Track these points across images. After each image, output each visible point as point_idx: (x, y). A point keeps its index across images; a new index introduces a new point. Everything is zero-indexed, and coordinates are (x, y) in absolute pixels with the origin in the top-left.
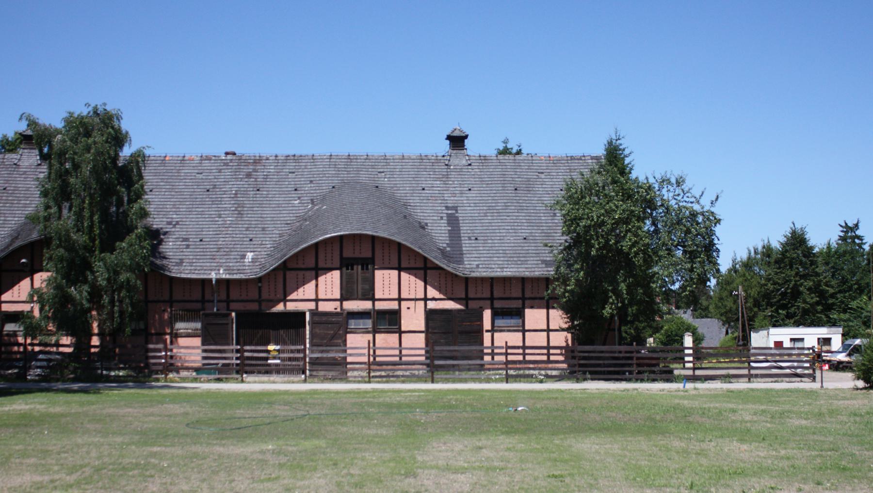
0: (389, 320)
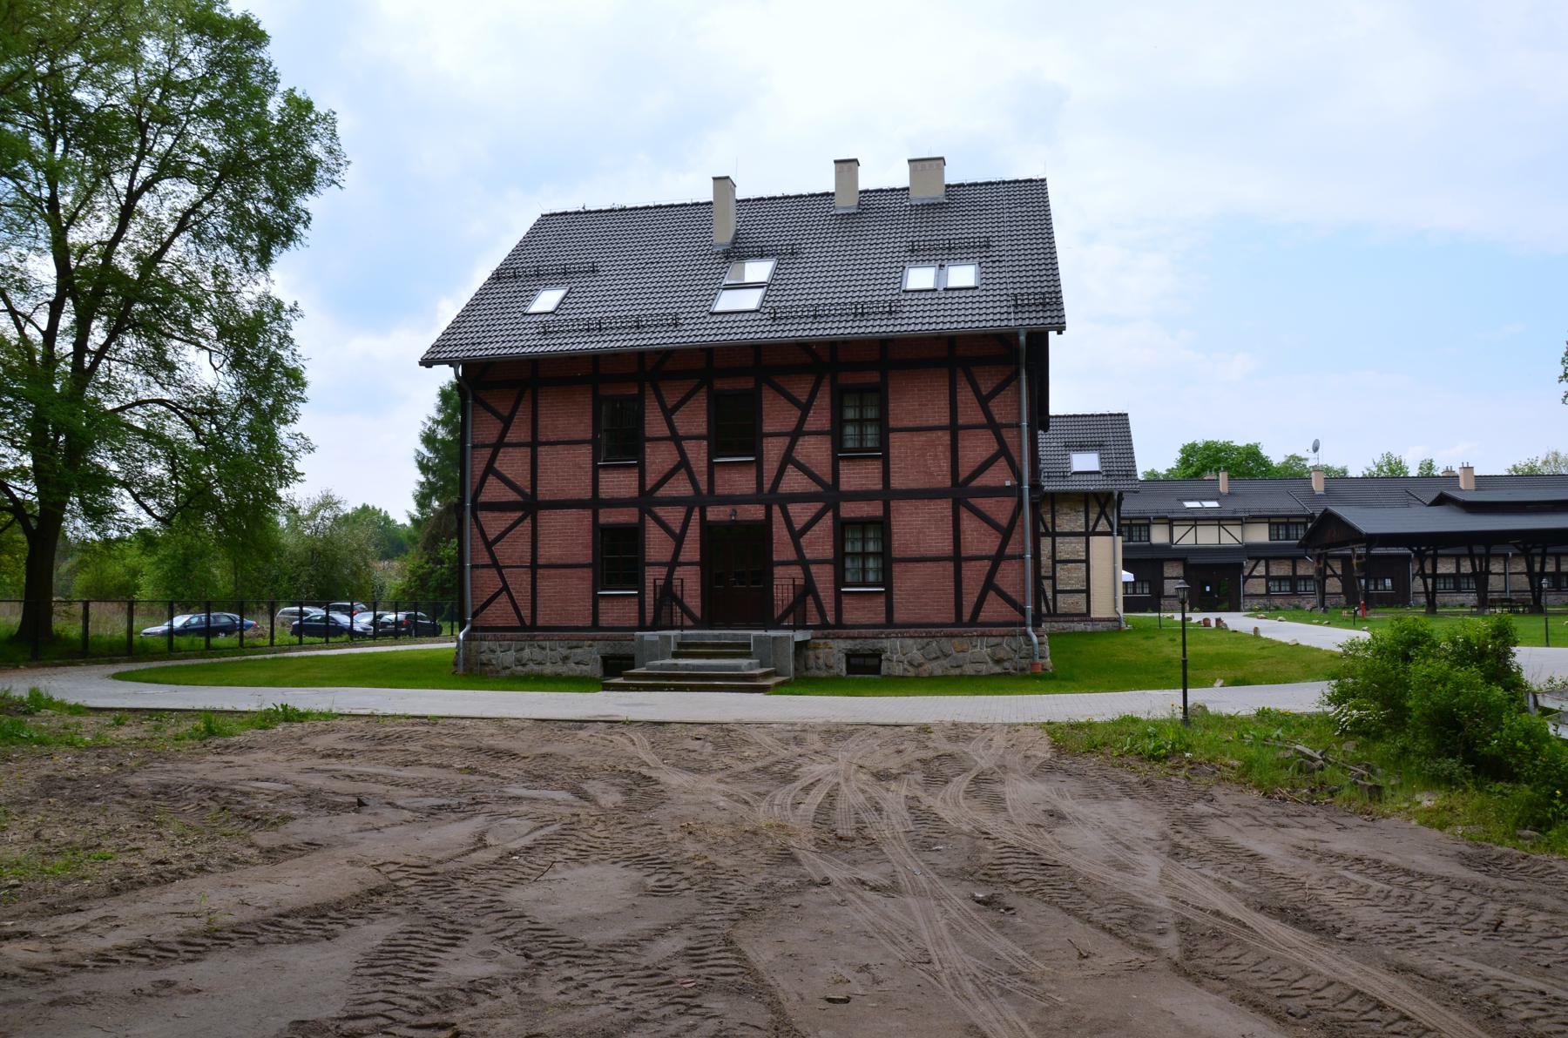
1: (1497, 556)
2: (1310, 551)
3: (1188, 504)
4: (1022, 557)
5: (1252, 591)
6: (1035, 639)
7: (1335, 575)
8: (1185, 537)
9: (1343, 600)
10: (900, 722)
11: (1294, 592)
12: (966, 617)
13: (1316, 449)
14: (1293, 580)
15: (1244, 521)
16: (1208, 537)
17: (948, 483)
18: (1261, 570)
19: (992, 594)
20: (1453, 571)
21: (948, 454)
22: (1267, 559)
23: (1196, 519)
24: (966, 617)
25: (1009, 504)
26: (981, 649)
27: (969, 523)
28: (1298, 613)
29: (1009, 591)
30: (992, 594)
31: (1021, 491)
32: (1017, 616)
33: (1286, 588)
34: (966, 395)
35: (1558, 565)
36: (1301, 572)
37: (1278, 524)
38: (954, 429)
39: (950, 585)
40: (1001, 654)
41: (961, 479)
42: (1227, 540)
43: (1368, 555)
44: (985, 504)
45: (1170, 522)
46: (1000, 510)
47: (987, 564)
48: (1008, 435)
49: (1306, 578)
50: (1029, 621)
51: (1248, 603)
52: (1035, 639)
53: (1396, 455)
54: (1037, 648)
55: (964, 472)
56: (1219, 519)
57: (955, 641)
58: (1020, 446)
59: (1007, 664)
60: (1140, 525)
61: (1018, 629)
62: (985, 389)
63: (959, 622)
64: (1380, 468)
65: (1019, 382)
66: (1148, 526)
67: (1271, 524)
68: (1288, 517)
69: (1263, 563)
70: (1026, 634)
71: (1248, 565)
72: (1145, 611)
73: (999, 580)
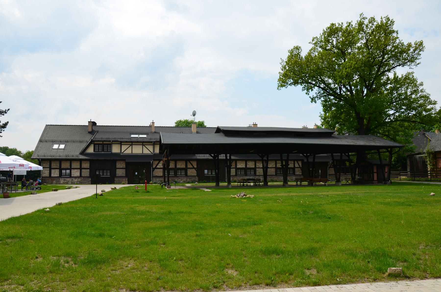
3: (132, 136)
5: (157, 175)
7: (194, 168)
8: (127, 150)
9: (197, 179)
13: (194, 115)
16: (137, 150)
20: (244, 166)
23: (132, 142)
33: (243, 172)
36: (179, 166)
42: (146, 152)
45: (121, 143)
49: (181, 169)
51: (154, 180)
60: (108, 144)
66: (111, 145)
68: (103, 141)
72: (209, 182)
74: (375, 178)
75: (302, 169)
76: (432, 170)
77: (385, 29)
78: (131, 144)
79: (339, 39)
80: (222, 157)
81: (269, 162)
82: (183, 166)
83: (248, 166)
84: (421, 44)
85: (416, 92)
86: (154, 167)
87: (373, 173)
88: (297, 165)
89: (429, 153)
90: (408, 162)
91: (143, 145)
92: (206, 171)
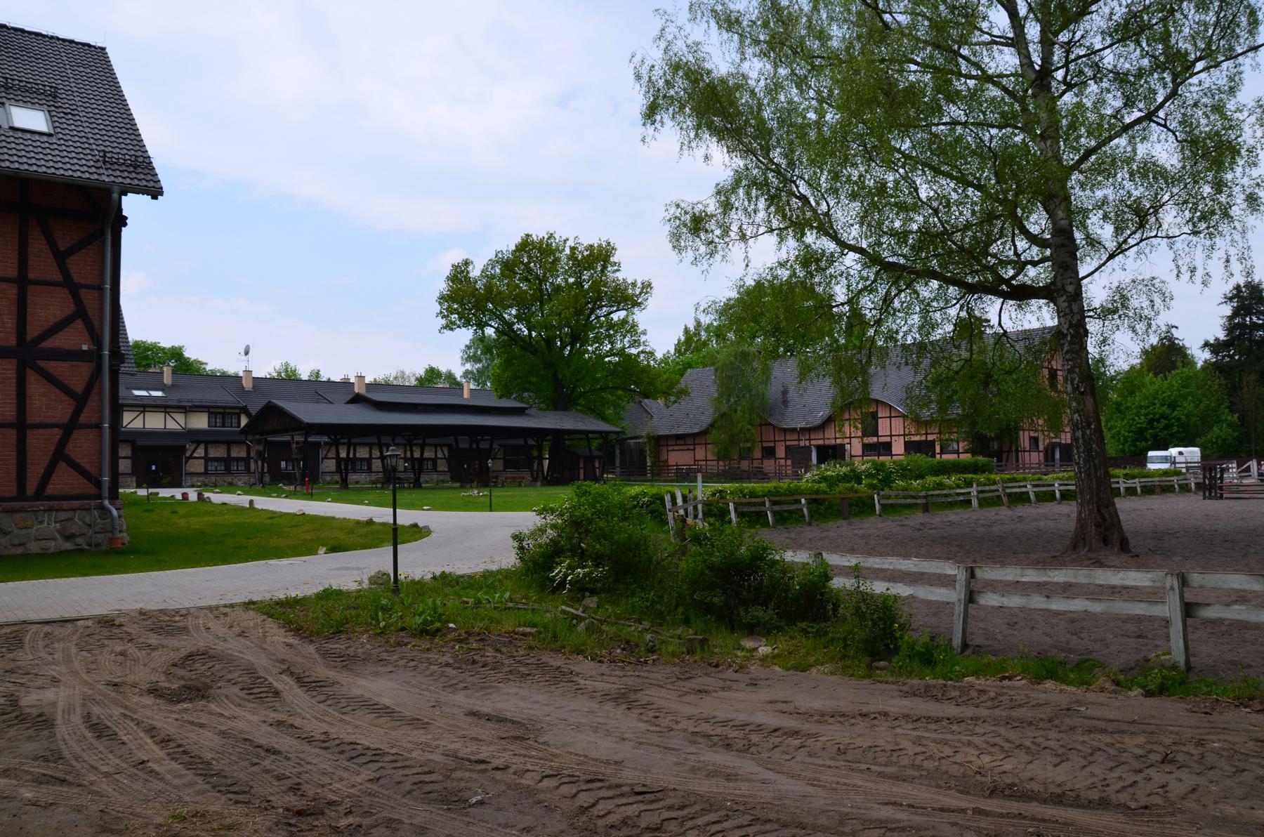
0: (886, 448)
1: (430, 445)
2: (250, 437)
4: (98, 426)
5: (192, 470)
6: (115, 512)
10: (67, 615)
11: (228, 471)
12: (31, 489)
14: (227, 461)
15: (187, 409)
16: (155, 422)
17: (13, 341)
18: (200, 452)
19: (62, 465)
21: (14, 309)
22: (207, 443)
23: (144, 406)
24: (31, 489)
25: (85, 369)
26: (49, 525)
27: (36, 387)
28: (231, 488)
29: (83, 462)
30: (62, 465)
31: (100, 357)
32: (91, 489)
34: (38, 246)
35: (422, 453)
36: (234, 454)
37: (216, 413)
38: (23, 283)
39: (11, 455)
40: (73, 529)
41: (29, 338)
42: (172, 425)
43: (306, 442)
44: (58, 368)
46: (76, 375)
47: (57, 434)
48: (87, 298)
49: (238, 460)
50: (106, 493)
51: (189, 480)
52: (115, 512)
53: (292, 365)
54: (117, 522)
55: (33, 331)
56: (166, 407)
57: (17, 516)
58: (101, 309)
59: (79, 540)
61: (93, 503)
62: (63, 245)
63: (21, 494)
64: (279, 373)
65: (104, 242)
67: (210, 413)
68: (225, 408)
69: (202, 446)
70: (102, 508)
71: (190, 447)
73: (72, 449)
74: (582, 476)
75: (448, 460)
76: (654, 464)
77: (601, 256)
78: (373, 440)
79: (534, 255)
80: (312, 439)
81: (427, 449)
82: (243, 454)
83: (358, 455)
84: (649, 285)
85: (635, 343)
86: (188, 454)
87: (578, 469)
88: (440, 455)
89: (650, 438)
90: (618, 452)
91: (166, 412)
92: (283, 464)
